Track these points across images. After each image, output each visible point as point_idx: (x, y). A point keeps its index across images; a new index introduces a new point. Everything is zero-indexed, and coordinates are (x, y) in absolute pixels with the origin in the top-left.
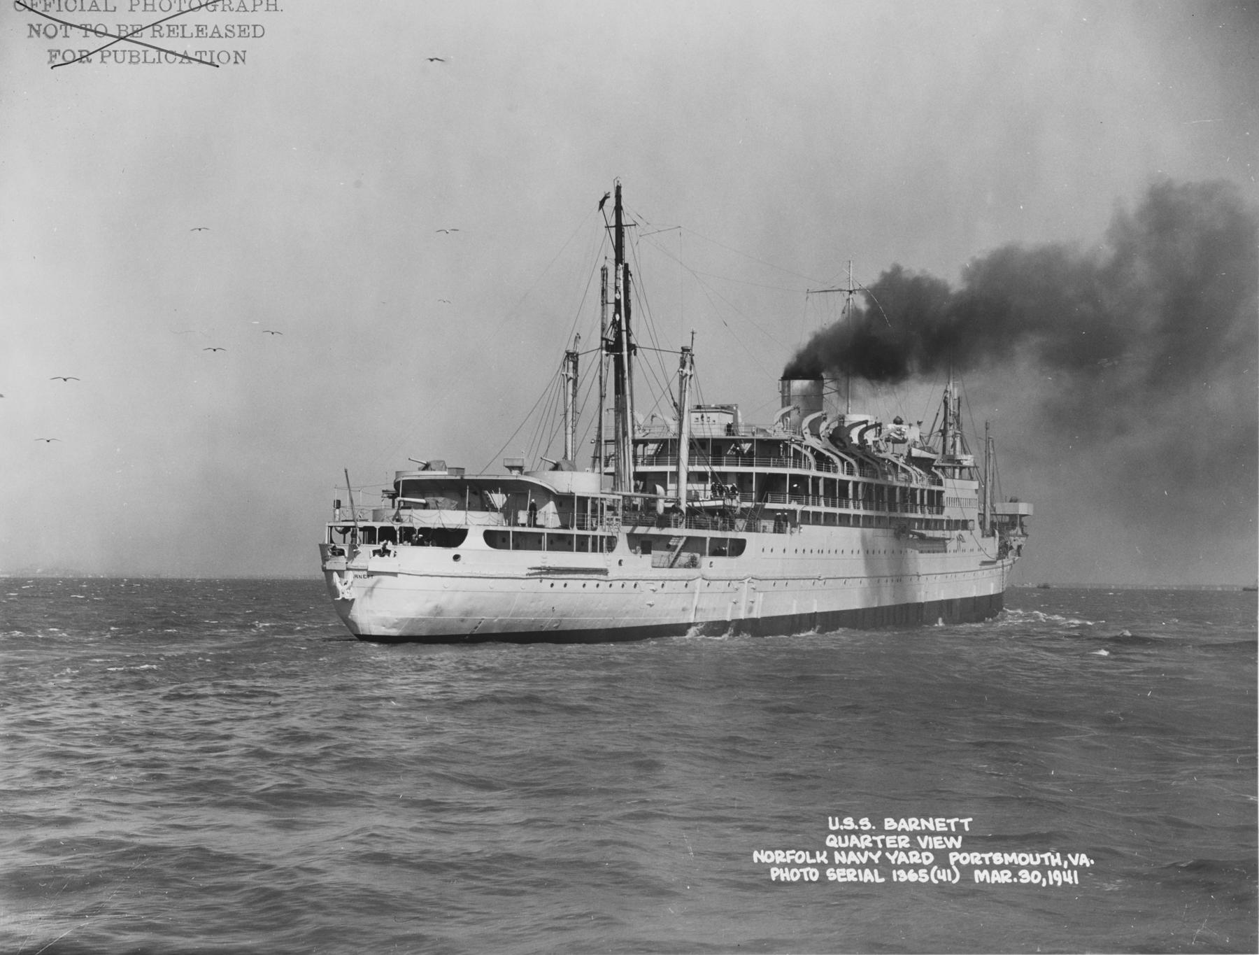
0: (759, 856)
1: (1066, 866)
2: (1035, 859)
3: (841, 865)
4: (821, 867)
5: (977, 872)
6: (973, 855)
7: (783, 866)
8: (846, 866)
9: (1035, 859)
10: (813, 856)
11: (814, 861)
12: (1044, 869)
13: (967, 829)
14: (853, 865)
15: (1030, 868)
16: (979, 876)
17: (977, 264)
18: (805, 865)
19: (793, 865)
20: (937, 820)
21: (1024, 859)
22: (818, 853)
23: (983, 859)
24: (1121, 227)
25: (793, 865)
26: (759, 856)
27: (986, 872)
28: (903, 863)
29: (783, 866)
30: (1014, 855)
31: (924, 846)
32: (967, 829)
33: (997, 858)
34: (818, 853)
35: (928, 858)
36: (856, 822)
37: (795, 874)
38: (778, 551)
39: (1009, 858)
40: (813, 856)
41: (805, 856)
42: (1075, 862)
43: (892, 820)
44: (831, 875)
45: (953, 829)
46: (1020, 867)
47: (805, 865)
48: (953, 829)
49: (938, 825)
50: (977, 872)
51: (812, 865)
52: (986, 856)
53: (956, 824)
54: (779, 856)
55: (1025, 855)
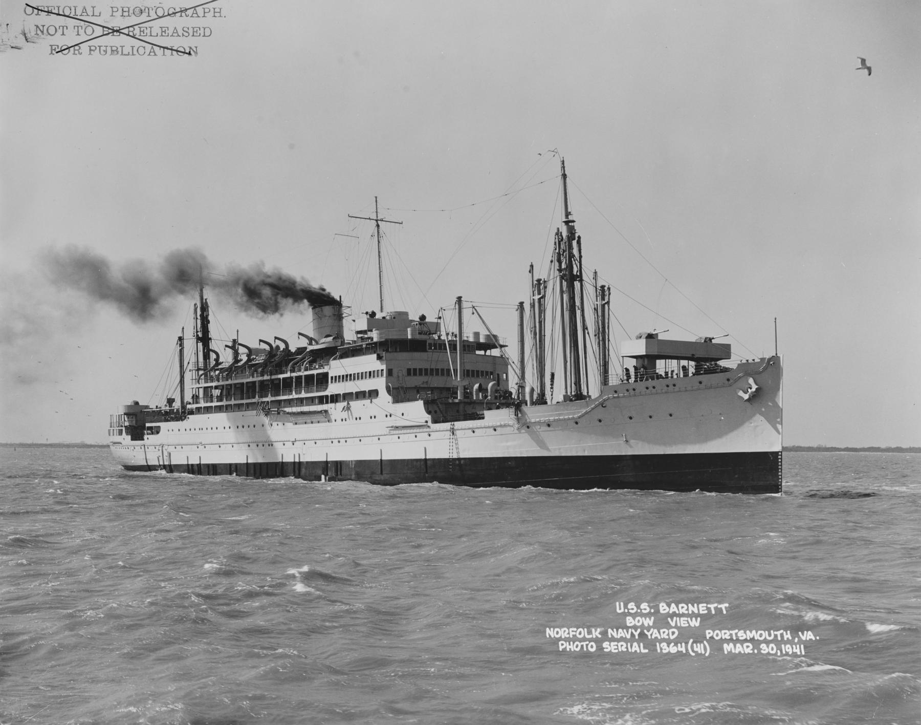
0: (550, 633)
1: (796, 640)
2: (770, 635)
3: (613, 639)
4: (599, 642)
5: (725, 646)
6: (723, 632)
7: (567, 640)
8: (618, 640)
9: (770, 635)
10: (590, 633)
11: (590, 636)
12: (778, 642)
13: (725, 612)
14: (622, 639)
15: (767, 642)
16: (727, 648)
17: (204, 257)
18: (584, 639)
19: (574, 639)
20: (701, 605)
21: (761, 635)
22: (593, 630)
23: (731, 635)
24: (762, 359)
25: (574, 639)
26: (550, 633)
27: (731, 645)
28: (656, 638)
29: (567, 640)
30: (754, 632)
31: (673, 624)
32: (725, 612)
33: (741, 635)
34: (593, 630)
35: (592, 647)
36: (638, 607)
37: (577, 646)
38: (176, 430)
39: (749, 635)
40: (590, 633)
41: (584, 632)
42: (804, 638)
43: (664, 605)
44: (609, 647)
45: (713, 612)
46: (760, 642)
47: (584, 639)
48: (713, 612)
49: (701, 609)
50: (725, 646)
51: (590, 640)
52: (733, 632)
53: (716, 608)
54: (563, 633)
55: (762, 632)
